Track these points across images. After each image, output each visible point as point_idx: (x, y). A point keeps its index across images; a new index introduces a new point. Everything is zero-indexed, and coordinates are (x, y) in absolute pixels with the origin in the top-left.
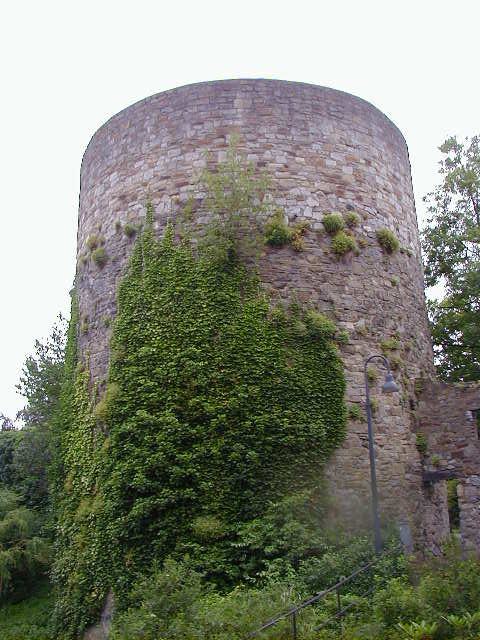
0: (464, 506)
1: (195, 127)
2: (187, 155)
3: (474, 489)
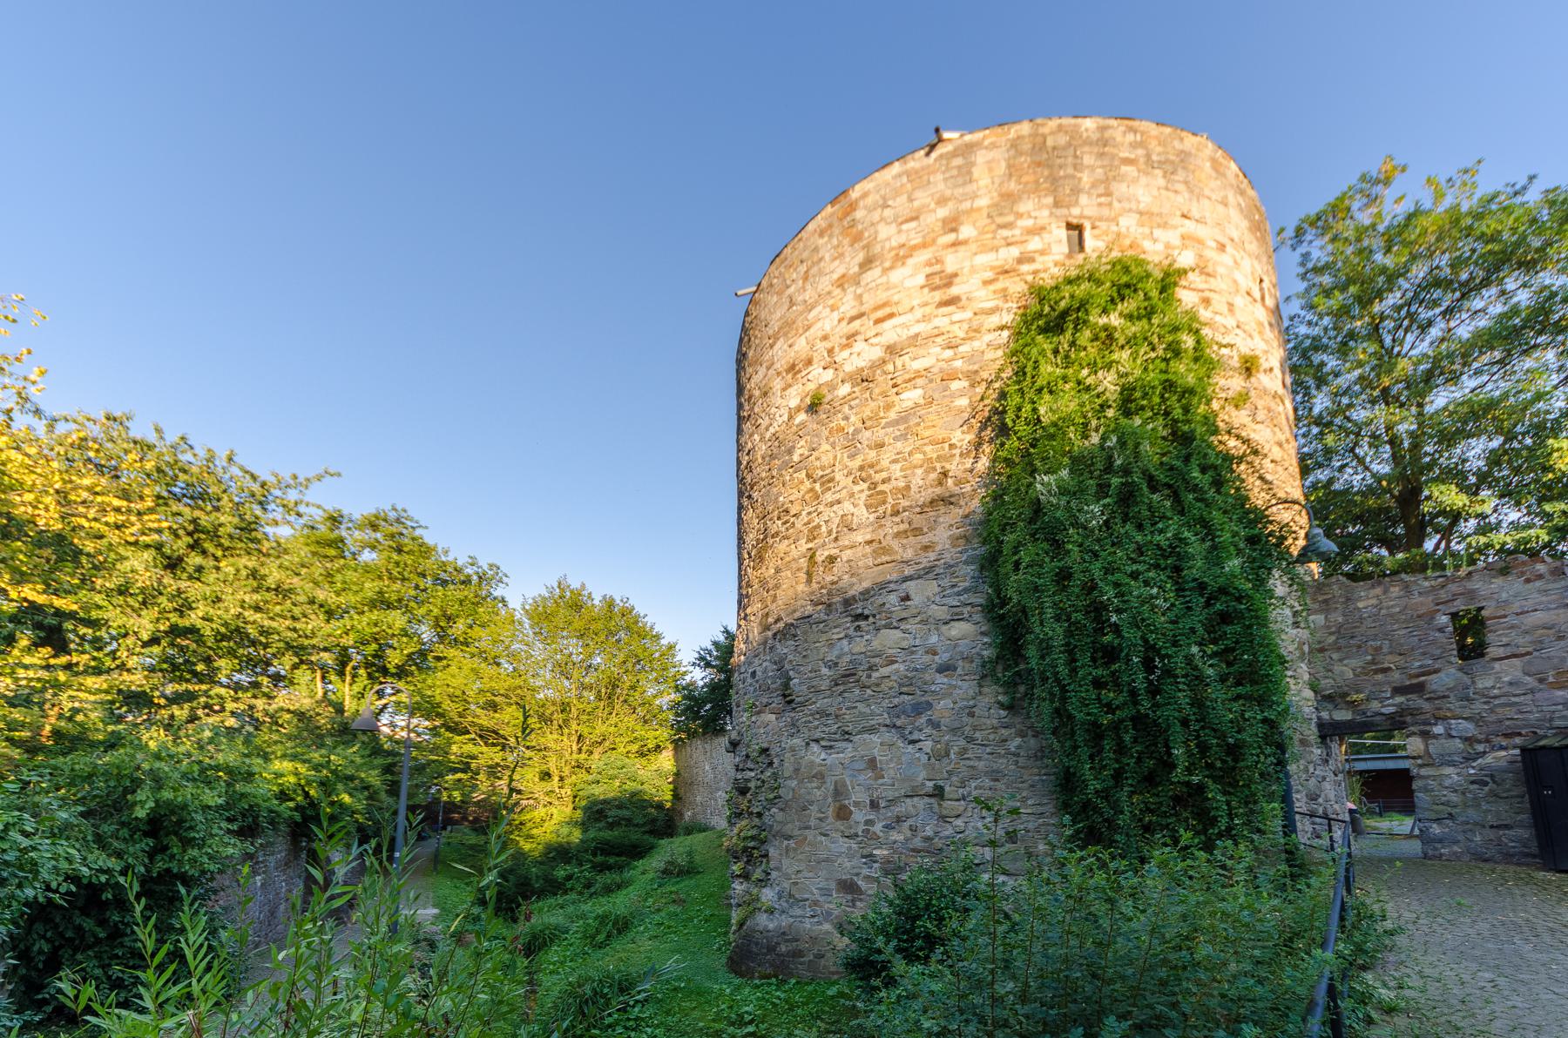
1: (905, 227)
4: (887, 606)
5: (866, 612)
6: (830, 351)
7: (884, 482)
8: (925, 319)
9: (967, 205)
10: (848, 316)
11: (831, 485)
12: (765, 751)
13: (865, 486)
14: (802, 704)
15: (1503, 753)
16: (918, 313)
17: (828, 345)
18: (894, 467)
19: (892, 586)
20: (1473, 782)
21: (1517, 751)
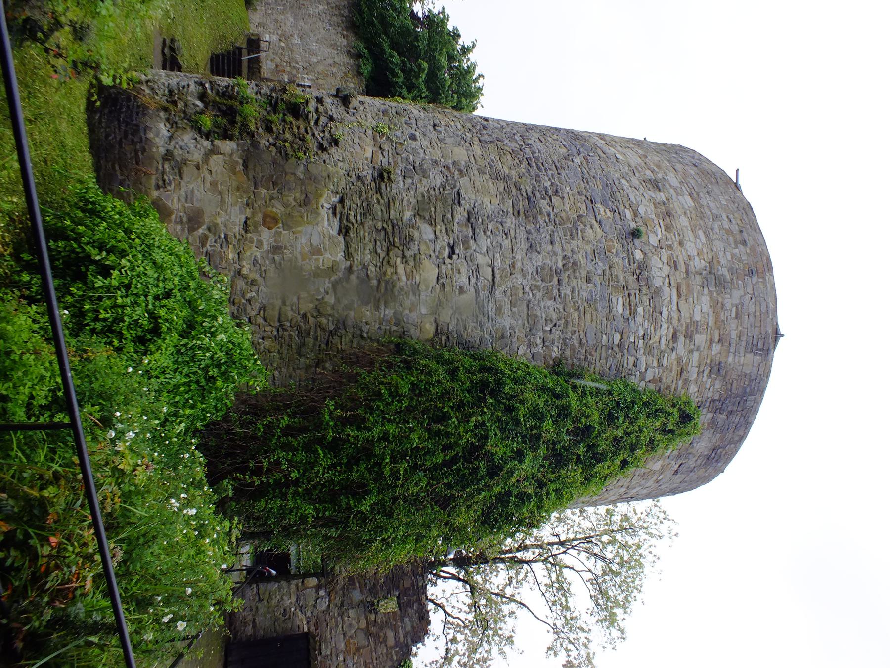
0: (293, 587)
1: (734, 309)
2: (708, 298)
3: (312, 602)
4: (458, 276)
5: (455, 257)
6: (670, 247)
7: (559, 281)
8: (670, 320)
9: (732, 350)
10: (691, 263)
11: (568, 237)
12: (335, 142)
13: (560, 264)
14: (378, 190)
15: (305, 623)
16: (675, 315)
17: (676, 245)
18: (569, 288)
19: (473, 280)
20: (285, 610)
21: (306, 630)
